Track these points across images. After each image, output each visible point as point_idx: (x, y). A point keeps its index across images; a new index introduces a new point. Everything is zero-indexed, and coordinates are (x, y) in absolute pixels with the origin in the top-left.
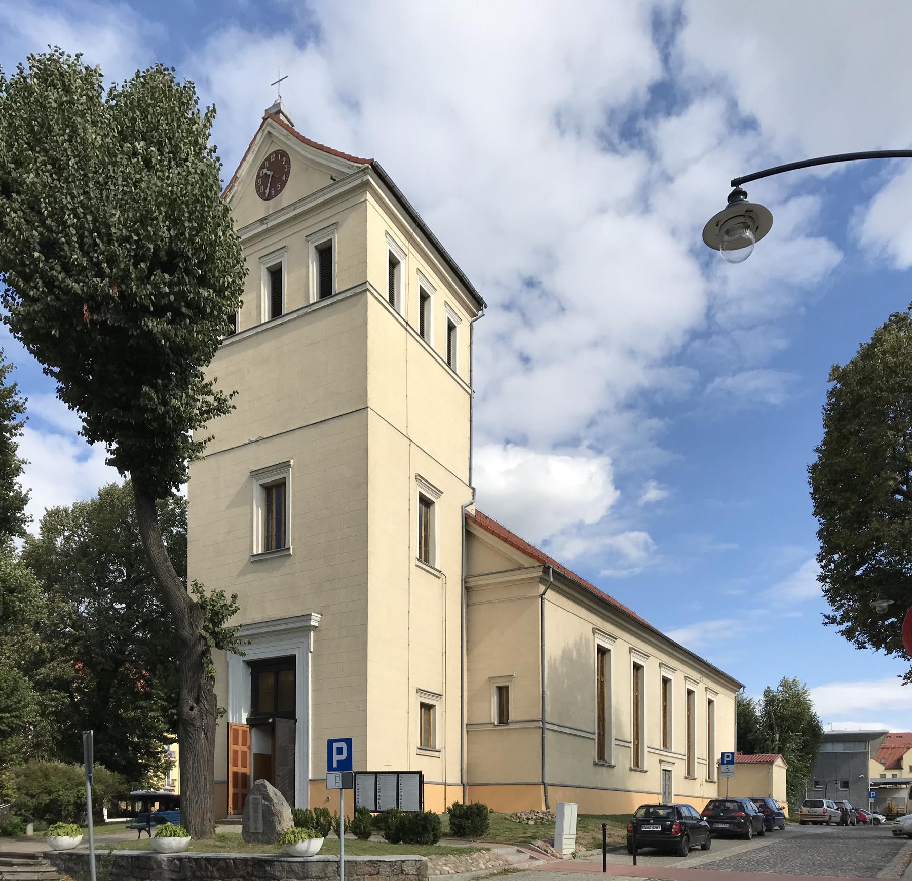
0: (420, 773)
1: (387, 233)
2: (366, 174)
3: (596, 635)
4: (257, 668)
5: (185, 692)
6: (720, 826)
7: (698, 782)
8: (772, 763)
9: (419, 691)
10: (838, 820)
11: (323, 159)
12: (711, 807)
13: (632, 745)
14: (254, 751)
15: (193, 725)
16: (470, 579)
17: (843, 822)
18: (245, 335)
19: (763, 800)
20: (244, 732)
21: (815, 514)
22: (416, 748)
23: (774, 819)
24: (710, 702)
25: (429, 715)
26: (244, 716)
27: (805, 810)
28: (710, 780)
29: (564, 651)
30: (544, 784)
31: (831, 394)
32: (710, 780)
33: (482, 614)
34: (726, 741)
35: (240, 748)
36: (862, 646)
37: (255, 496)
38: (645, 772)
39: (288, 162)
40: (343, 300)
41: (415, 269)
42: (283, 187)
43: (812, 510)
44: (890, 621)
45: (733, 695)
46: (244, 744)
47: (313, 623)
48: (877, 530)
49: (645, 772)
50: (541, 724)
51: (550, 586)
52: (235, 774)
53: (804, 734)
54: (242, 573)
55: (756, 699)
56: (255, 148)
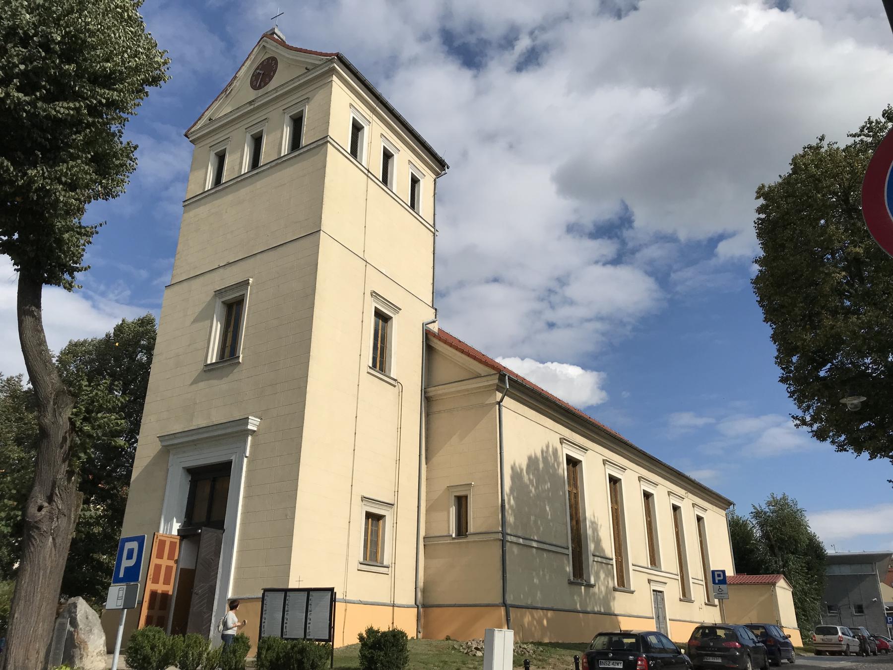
0: (331, 590)
1: (351, 105)
2: (332, 63)
3: (564, 445)
4: (196, 475)
5: (37, 488)
6: (711, 660)
7: (696, 605)
8: (774, 584)
9: (364, 498)
10: (857, 649)
11: (301, 57)
12: (699, 635)
13: (614, 562)
14: (181, 566)
15: (38, 528)
16: (429, 389)
17: (863, 651)
18: (226, 185)
19: (763, 627)
20: (173, 544)
21: (766, 320)
22: (357, 563)
23: (779, 650)
24: (699, 519)
25: (377, 526)
26: (176, 526)
27: (819, 638)
28: (709, 603)
29: (530, 458)
30: (504, 604)
31: (760, 210)
32: (709, 603)
33: (441, 422)
34: (723, 559)
35: (165, 562)
36: (841, 448)
37: (216, 310)
38: (632, 592)
39: (276, 64)
40: (308, 151)
41: (377, 135)
42: (270, 80)
43: (763, 316)
44: (866, 424)
45: (724, 513)
46: (170, 557)
47: (250, 427)
48: (832, 327)
49: (632, 592)
50: (500, 536)
51: (506, 393)
52: (154, 594)
53: (806, 554)
54: (195, 382)
55: (744, 512)
56: (252, 57)
